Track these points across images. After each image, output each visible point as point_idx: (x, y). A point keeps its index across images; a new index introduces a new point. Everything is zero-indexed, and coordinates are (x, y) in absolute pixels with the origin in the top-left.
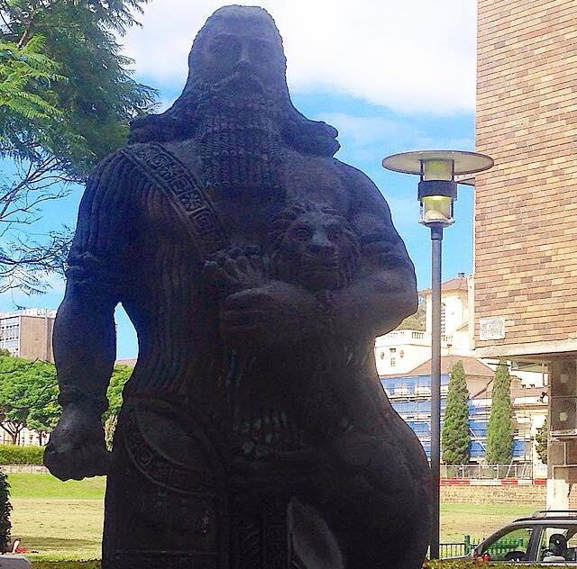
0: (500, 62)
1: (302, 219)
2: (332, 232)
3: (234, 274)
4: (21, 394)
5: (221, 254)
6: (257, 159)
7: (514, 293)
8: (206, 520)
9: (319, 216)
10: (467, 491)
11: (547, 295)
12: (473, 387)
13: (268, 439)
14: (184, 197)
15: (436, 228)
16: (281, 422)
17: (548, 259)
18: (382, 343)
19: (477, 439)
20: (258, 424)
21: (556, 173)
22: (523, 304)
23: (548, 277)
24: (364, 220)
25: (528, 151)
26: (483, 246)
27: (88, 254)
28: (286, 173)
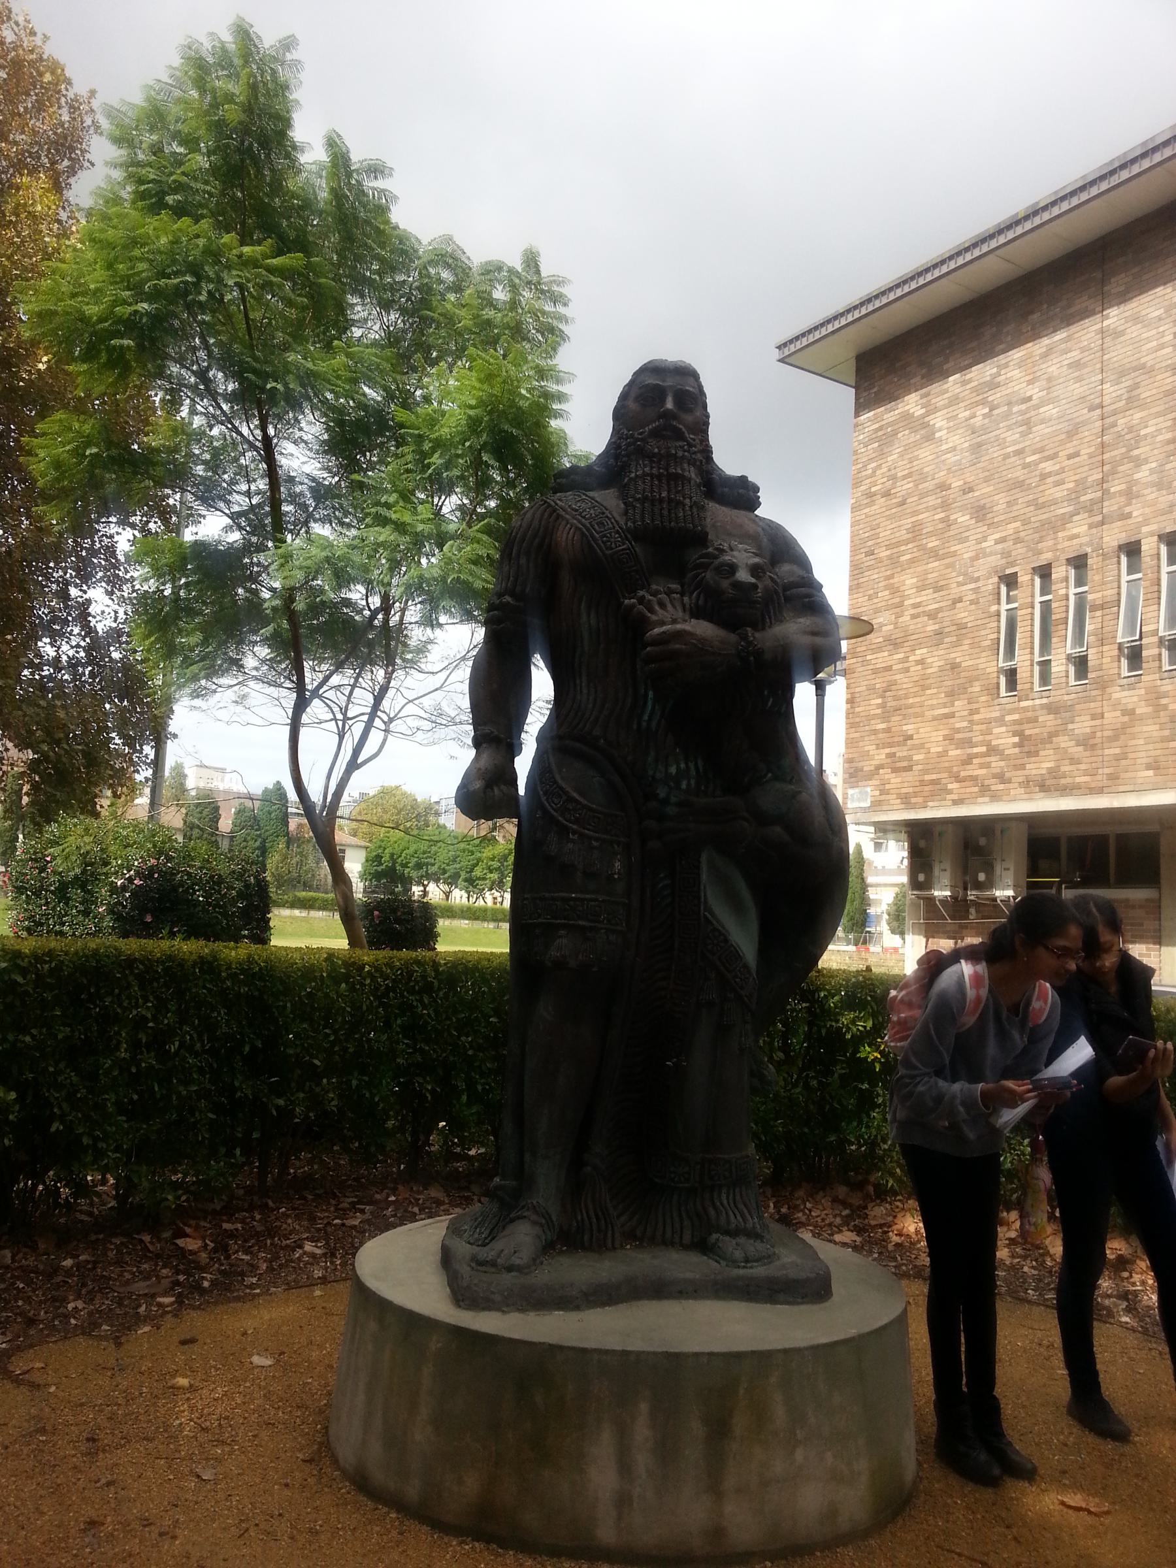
0: (869, 568)
2: (755, 570)
3: (652, 611)
4: (454, 861)
6: (679, 503)
7: (879, 767)
8: (617, 864)
9: (742, 557)
11: (909, 769)
13: (684, 786)
14: (605, 536)
16: (697, 769)
17: (911, 737)
20: (673, 770)
21: (921, 662)
22: (887, 776)
23: (910, 753)
24: (786, 570)
25: (894, 644)
27: (507, 599)
28: (708, 520)
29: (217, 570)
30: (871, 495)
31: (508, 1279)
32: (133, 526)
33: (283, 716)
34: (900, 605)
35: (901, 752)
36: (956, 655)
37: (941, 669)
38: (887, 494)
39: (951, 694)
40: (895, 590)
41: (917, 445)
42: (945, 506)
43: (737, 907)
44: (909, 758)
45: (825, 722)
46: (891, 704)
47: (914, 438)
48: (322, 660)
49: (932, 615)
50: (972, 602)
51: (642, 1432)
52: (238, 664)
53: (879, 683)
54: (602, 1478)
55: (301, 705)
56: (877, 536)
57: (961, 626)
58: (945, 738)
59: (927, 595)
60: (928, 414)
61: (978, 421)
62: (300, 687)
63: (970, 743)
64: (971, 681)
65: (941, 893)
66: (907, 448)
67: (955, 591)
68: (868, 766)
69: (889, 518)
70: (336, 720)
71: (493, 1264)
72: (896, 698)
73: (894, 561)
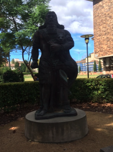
0: (96, 26)
1: (59, 36)
2: (62, 37)
5: (49, 41)
7: (99, 51)
9: (61, 36)
10: (96, 74)
11: (102, 51)
12: (97, 63)
15: (87, 43)
18: (71, 50)
19: (97, 68)
20: (55, 61)
21: (103, 37)
25: (100, 35)
26: (95, 46)
27: (34, 43)
29: (10, 36)
30: (96, 16)
31: (41, 117)
32: (1, 30)
33: (22, 53)
34: (100, 30)
35: (101, 49)
36: (108, 36)
37: (106, 38)
38: (98, 16)
39: (108, 41)
40: (99, 29)
41: (102, 9)
42: (106, 17)
43: (64, 75)
44: (102, 50)
45: (77, 54)
46: (100, 43)
47: (101, 8)
48: (25, 46)
49: (105, 31)
50: (110, 29)
51: (54, 130)
52: (15, 47)
53: (98, 41)
54: (51, 135)
55: (23, 52)
56: (97, 22)
57: (108, 32)
58: (107, 47)
59: (104, 29)
60: (103, 4)
61: (109, 5)
62: (23, 50)
63: (110, 47)
64: (110, 39)
65: (107, 66)
66: (100, 9)
67: (107, 28)
68: (97, 51)
69: (98, 19)
70: (28, 53)
71: (39, 115)
72: (100, 42)
73: (99, 25)
